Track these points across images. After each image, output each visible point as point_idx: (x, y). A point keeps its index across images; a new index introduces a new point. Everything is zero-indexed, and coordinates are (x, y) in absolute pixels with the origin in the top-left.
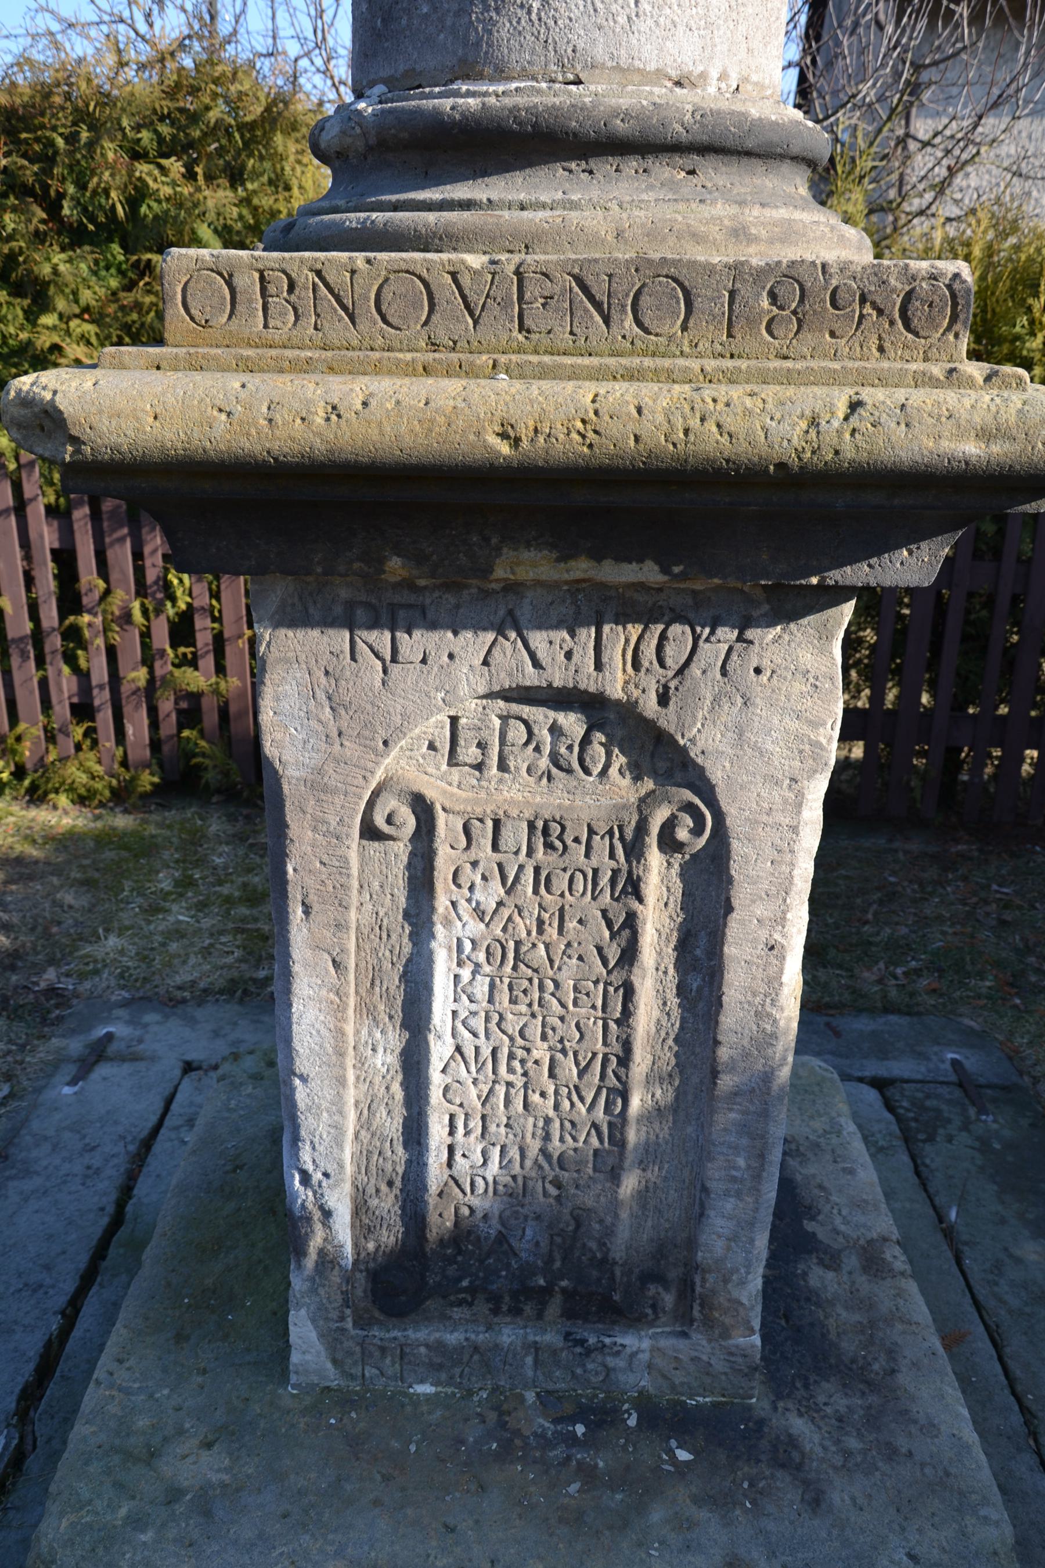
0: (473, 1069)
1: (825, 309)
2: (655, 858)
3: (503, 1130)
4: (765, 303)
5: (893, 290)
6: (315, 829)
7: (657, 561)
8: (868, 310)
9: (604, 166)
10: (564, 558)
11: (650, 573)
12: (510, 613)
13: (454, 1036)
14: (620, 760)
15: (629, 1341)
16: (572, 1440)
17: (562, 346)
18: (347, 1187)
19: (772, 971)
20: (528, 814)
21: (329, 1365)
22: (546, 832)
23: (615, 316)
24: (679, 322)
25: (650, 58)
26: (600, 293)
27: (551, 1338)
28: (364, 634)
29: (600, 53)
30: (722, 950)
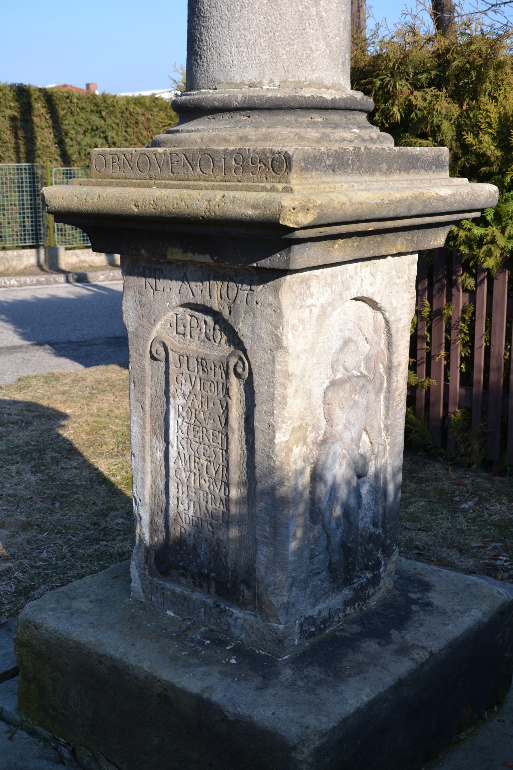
0: (183, 464)
1: (249, 164)
2: (233, 378)
3: (194, 494)
4: (233, 163)
5: (268, 158)
6: (136, 353)
7: (210, 255)
8: (262, 165)
9: (220, 116)
10: (185, 252)
11: (206, 259)
12: (185, 274)
13: (177, 447)
14: (225, 338)
15: (237, 612)
16: (202, 644)
17: (181, 177)
18: (148, 508)
19: (271, 437)
20: (195, 356)
21: (141, 591)
22: (202, 362)
23: (194, 168)
24: (211, 169)
25: (237, 79)
26: (191, 159)
27: (210, 601)
28: (148, 279)
29: (222, 79)
30: (253, 425)
